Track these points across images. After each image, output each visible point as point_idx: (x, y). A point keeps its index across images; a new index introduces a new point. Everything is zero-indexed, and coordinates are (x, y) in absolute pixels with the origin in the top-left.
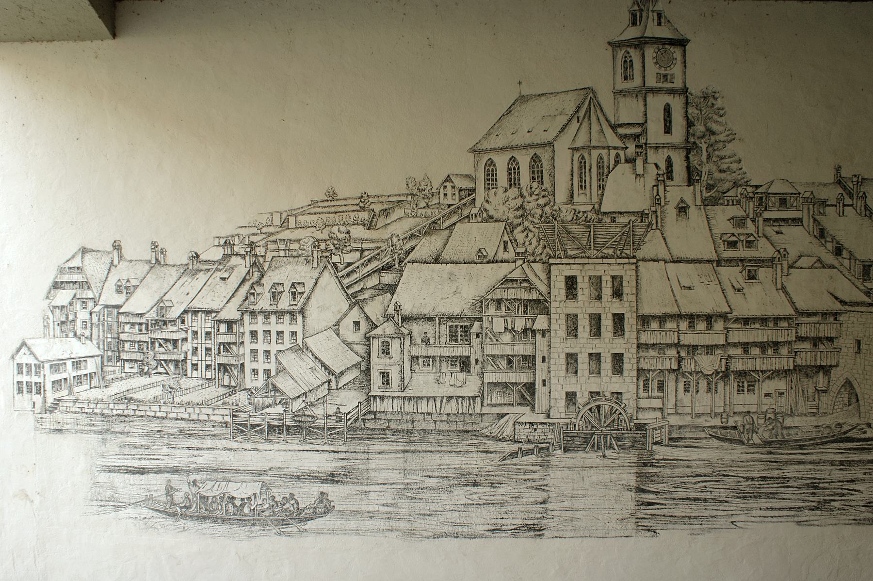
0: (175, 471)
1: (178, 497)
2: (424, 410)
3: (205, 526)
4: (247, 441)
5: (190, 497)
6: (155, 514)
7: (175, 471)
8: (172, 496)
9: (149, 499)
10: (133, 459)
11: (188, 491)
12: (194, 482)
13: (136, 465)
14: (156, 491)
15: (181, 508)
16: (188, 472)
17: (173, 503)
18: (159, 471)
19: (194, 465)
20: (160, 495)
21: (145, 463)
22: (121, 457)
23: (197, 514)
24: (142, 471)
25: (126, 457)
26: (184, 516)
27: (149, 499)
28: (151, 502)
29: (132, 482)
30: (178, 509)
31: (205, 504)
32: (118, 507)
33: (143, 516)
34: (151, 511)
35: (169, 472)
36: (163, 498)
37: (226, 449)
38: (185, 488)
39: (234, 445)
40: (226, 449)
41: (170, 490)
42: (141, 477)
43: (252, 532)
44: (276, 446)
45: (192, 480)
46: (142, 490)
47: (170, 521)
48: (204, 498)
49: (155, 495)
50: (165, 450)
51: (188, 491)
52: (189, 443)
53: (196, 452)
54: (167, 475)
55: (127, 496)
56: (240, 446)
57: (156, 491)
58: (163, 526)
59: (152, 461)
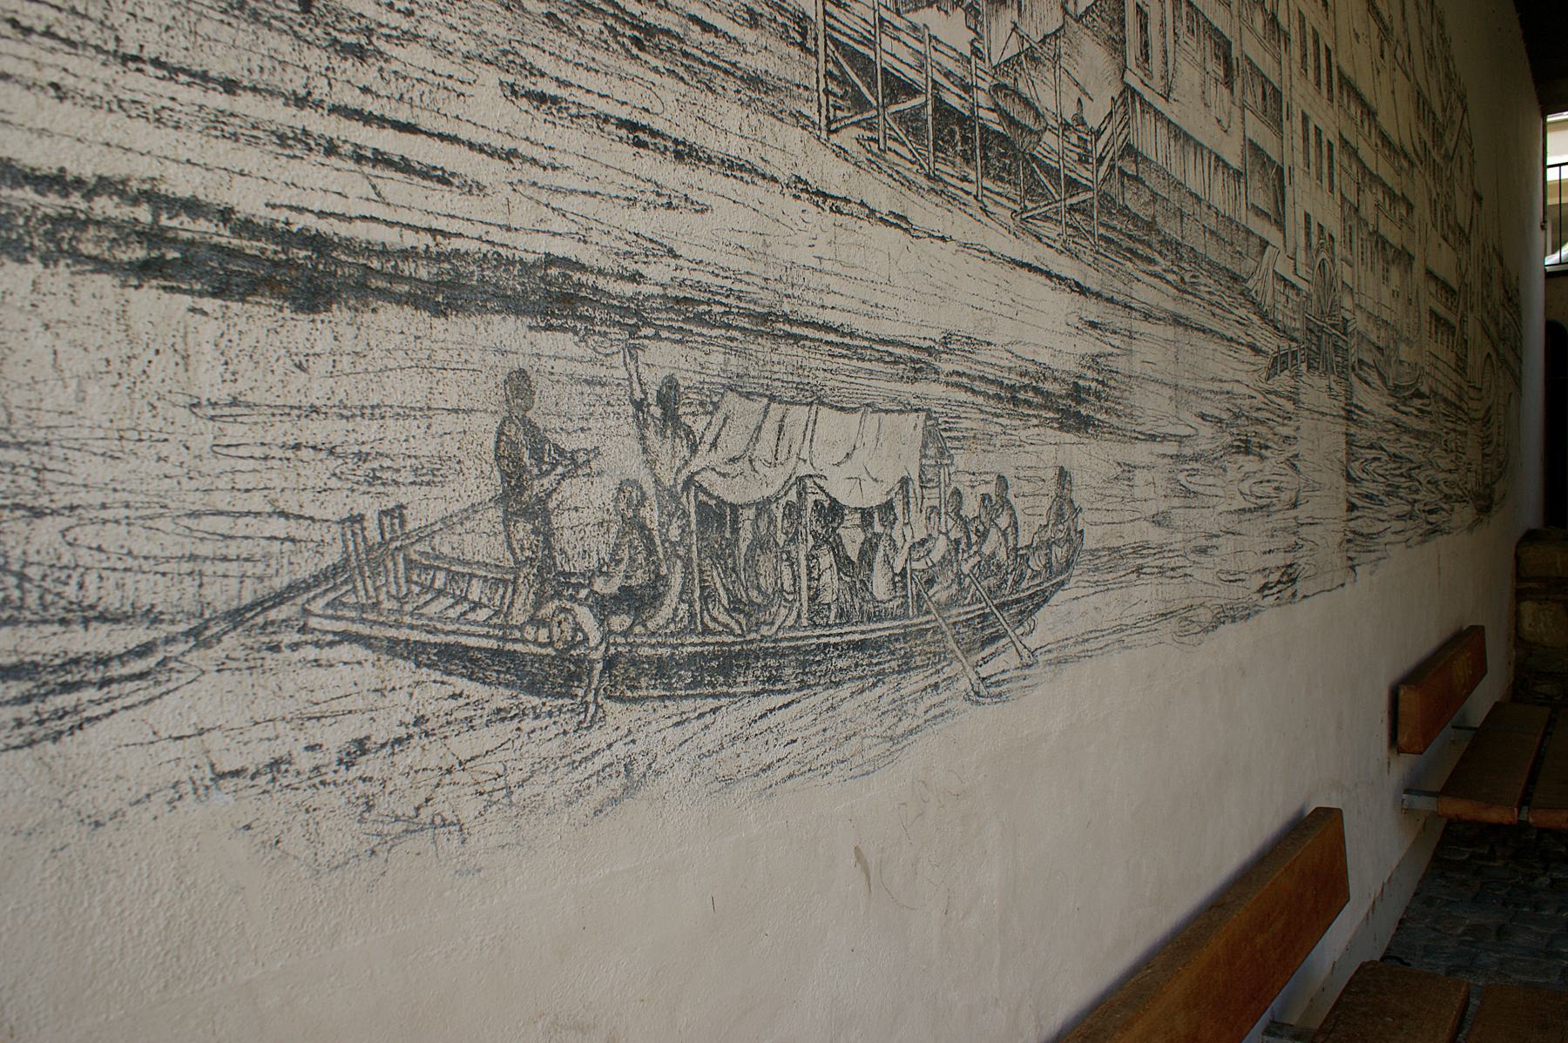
0: (556, 296)
1: (583, 513)
2: (152, 32)
3: (730, 719)
4: (875, 162)
5: (651, 515)
6: (432, 692)
7: (556, 296)
8: (539, 513)
9: (375, 558)
10: (217, 124)
11: (634, 467)
12: (669, 396)
13: (249, 201)
14: (429, 476)
15: (604, 607)
16: (634, 318)
17: (554, 581)
18: (448, 289)
19: (658, 271)
20: (457, 508)
21: (324, 194)
22: (87, 71)
23: (691, 645)
24: (305, 272)
25: (145, 85)
26: (626, 675)
27: (375, 558)
28: (389, 586)
29: (209, 382)
30: (586, 617)
31: (721, 556)
32: (69, 673)
33: (336, 737)
34: (402, 672)
35: (513, 305)
36: (483, 543)
37: (802, 187)
38: (621, 452)
39: (833, 174)
40: (802, 187)
41: (526, 467)
42: (302, 330)
43: (899, 708)
44: (959, 224)
45: (654, 379)
46: (317, 471)
47: (543, 734)
48: (717, 515)
49: (424, 507)
50: (488, 108)
51: (634, 467)
52: (635, 94)
53: (673, 175)
54: (507, 329)
55: (168, 541)
56: (882, 196)
57: (429, 476)
58: (498, 792)
59: (395, 185)
